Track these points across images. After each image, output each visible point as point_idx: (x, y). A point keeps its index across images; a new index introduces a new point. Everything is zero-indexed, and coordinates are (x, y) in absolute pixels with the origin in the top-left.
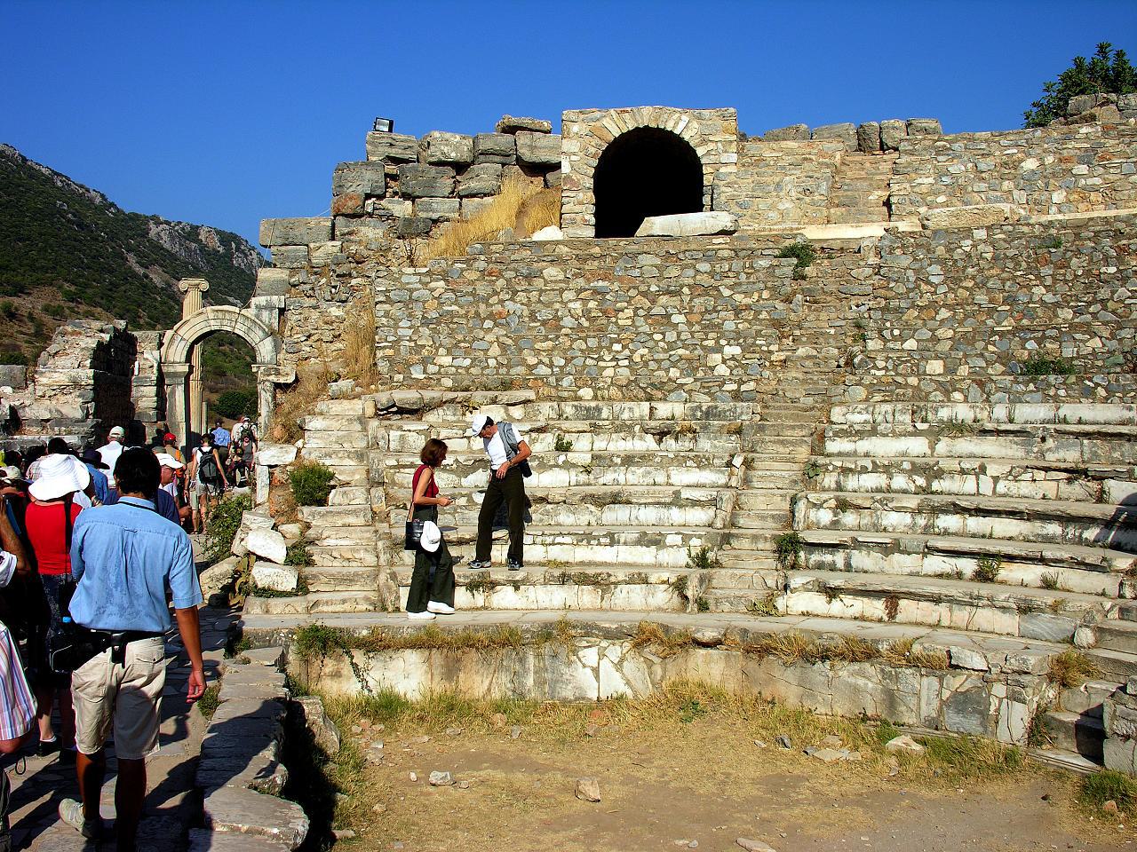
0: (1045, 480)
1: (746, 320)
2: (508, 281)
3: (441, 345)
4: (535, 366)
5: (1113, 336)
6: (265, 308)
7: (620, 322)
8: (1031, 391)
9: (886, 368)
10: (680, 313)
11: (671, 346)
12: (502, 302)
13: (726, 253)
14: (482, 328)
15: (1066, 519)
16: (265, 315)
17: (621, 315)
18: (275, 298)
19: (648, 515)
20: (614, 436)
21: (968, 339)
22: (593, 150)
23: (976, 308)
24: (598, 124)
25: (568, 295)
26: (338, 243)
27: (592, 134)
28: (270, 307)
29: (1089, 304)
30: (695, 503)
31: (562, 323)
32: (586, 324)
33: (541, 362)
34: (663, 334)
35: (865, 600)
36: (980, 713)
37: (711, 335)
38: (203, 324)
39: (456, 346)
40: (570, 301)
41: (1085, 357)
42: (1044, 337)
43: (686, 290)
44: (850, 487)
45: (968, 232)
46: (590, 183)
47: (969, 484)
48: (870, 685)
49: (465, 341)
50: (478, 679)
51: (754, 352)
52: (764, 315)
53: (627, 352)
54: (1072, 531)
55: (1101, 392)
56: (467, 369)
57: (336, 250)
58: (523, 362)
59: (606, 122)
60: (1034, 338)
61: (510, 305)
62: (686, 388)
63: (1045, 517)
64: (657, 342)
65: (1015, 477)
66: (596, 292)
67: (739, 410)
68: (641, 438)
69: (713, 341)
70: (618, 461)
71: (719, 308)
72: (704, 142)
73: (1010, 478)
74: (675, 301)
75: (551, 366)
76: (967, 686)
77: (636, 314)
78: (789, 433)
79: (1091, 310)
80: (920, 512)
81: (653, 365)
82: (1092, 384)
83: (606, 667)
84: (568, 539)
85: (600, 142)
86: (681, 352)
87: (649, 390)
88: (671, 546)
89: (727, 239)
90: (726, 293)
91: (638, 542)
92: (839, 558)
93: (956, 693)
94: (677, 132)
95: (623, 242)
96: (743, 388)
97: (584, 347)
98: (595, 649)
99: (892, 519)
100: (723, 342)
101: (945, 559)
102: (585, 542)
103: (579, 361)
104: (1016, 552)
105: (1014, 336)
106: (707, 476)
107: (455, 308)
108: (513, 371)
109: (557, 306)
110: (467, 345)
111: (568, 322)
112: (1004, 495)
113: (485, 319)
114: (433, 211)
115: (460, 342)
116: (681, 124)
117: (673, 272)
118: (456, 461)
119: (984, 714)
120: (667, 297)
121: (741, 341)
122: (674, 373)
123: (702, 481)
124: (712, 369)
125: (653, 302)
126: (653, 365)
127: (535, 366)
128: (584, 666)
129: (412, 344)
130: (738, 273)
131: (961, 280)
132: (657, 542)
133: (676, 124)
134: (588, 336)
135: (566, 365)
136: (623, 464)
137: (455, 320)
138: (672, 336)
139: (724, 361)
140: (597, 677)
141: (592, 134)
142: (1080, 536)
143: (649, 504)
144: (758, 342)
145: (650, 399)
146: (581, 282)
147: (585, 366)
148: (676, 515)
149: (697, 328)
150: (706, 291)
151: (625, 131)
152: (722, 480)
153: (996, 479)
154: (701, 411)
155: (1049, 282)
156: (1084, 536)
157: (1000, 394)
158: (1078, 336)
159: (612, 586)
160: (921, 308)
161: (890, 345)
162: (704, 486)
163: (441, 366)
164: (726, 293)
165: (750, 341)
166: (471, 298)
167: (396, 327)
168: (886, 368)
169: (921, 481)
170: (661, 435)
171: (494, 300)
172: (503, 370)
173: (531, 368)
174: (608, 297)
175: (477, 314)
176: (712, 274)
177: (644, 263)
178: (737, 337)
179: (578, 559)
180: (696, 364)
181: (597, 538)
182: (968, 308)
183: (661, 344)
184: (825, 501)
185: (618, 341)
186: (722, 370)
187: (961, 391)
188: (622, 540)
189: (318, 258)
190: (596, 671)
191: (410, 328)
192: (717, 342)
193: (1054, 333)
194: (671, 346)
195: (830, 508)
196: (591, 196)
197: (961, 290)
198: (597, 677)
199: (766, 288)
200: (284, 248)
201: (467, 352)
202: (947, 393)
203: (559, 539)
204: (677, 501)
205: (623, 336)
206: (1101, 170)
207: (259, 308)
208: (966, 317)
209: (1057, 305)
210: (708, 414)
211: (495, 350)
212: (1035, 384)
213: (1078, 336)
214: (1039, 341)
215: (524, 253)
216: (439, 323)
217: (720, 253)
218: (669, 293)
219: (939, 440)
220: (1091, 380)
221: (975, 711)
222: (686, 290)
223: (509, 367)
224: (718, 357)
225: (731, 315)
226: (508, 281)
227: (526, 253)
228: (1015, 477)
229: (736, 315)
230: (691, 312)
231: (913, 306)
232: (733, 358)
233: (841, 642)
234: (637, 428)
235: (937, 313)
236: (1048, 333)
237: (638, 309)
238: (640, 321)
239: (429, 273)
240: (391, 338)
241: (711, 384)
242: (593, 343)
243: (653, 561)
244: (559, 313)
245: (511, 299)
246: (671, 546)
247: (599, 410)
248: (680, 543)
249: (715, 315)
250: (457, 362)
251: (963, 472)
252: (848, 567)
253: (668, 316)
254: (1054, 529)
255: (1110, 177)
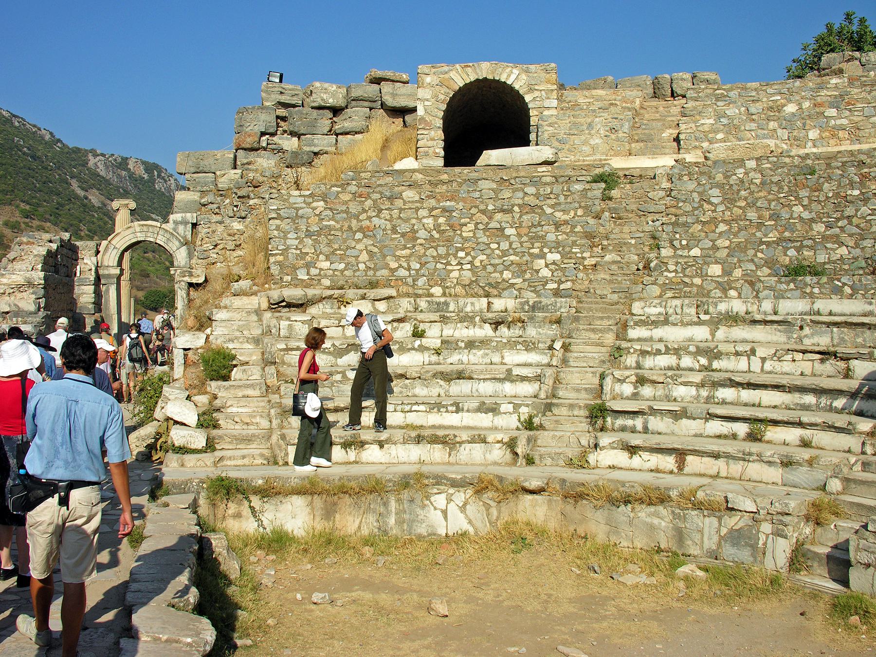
0: (803, 360)
1: (564, 233)
2: (375, 201)
3: (321, 253)
4: (396, 269)
5: (857, 245)
6: (181, 223)
7: (464, 234)
8: (792, 290)
9: (676, 271)
10: (512, 227)
11: (505, 253)
12: (369, 218)
13: (548, 179)
14: (354, 239)
15: (819, 392)
16: (181, 228)
17: (464, 228)
18: (189, 215)
19: (486, 388)
20: (459, 325)
21: (741, 248)
22: (442, 97)
23: (748, 223)
24: (446, 76)
25: (423, 213)
26: (239, 171)
27: (441, 84)
28: (184, 222)
29: (838, 220)
30: (524, 379)
31: (417, 235)
32: (437, 236)
33: (400, 266)
34: (498, 244)
35: (660, 456)
36: (751, 546)
37: (536, 245)
38: (131, 236)
39: (333, 253)
40: (424, 217)
41: (834, 262)
42: (802, 247)
43: (516, 209)
44: (647, 366)
45: (741, 162)
46: (439, 123)
47: (742, 364)
48: (663, 524)
49: (340, 249)
50: (350, 519)
51: (570, 258)
52: (578, 229)
53: (469, 258)
54: (824, 401)
55: (847, 290)
56: (342, 271)
57: (237, 176)
58: (386, 267)
59: (453, 74)
60: (794, 247)
61: (376, 221)
62: (517, 287)
63: (802, 390)
64: (493, 250)
65: (779, 358)
66: (444, 210)
67: (558, 305)
68: (481, 327)
69: (538, 250)
70: (462, 345)
71: (543, 223)
72: (531, 90)
73: (775, 358)
74: (508, 217)
75: (409, 269)
76: (741, 524)
77: (476, 228)
78: (598, 322)
79: (840, 224)
80: (703, 386)
81: (490, 269)
82: (840, 284)
83: (453, 509)
84: (422, 408)
85: (448, 91)
86: (512, 258)
87: (487, 288)
88: (505, 413)
89: (549, 168)
90: (549, 211)
91: (479, 410)
92: (639, 423)
93: (731, 531)
94: (509, 82)
95: (466, 170)
96: (562, 287)
97: (435, 254)
98: (444, 496)
99: (680, 391)
100: (546, 250)
101: (723, 423)
102: (436, 410)
103: (431, 266)
104: (780, 418)
105: (778, 245)
106: (533, 357)
107: (332, 223)
108: (378, 273)
109: (414, 221)
110: (342, 252)
111: (422, 234)
112: (770, 372)
113: (356, 232)
114: (315, 146)
115: (336, 250)
116: (513, 76)
117: (506, 194)
118: (333, 345)
119: (754, 547)
120: (501, 214)
121: (560, 249)
122: (507, 275)
123: (530, 361)
124: (537, 271)
125: (490, 218)
126: (490, 269)
127: (396, 269)
128: (435, 509)
129: (298, 252)
130: (558, 195)
131: (736, 201)
132: (494, 410)
133: (509, 76)
134: (438, 246)
135: (421, 268)
136: (466, 348)
137: (332, 232)
138: (505, 245)
139: (547, 266)
140: (446, 518)
141: (441, 84)
142: (831, 405)
143: (487, 379)
144: (574, 250)
145: (487, 295)
146: (433, 202)
147: (436, 269)
148: (508, 388)
149: (525, 239)
150: (533, 209)
151: (468, 81)
152: (545, 360)
153: (764, 360)
154: (529, 305)
155: (806, 202)
156: (834, 405)
157: (767, 292)
158: (829, 245)
159: (458, 445)
160: (704, 223)
161: (679, 252)
162: (530, 365)
163: (321, 269)
164: (549, 211)
165: (568, 249)
166: (345, 215)
167: (285, 238)
168: (676, 271)
169: (703, 361)
170: (497, 324)
171: (363, 216)
172: (371, 273)
173: (393, 271)
174: (454, 214)
175: (350, 228)
176: (537, 196)
177: (483, 187)
178: (557, 246)
179: (430, 423)
180: (524, 268)
181: (445, 406)
182: (741, 223)
183: (497, 252)
184: (627, 377)
185: (462, 250)
186: (545, 273)
187: (736, 289)
188: (465, 408)
189: (223, 183)
190: (445, 513)
191: (296, 239)
192: (541, 250)
193: (810, 243)
194: (505, 253)
195: (631, 383)
196: (440, 134)
197: (735, 209)
198: (446, 518)
199: (580, 207)
200: (196, 175)
201: (342, 258)
202: (725, 291)
203: (415, 408)
204: (509, 377)
205: (466, 245)
206: (847, 113)
207: (176, 223)
208: (740, 230)
209: (812, 220)
210: (534, 308)
211: (364, 257)
212: (795, 284)
213: (829, 245)
214: (798, 250)
215: (387, 179)
216: (319, 235)
217: (544, 179)
218: (502, 211)
219: (718, 328)
220: (839, 280)
221: (747, 544)
222: (516, 209)
223: (375, 270)
224: (542, 262)
225: (552, 228)
226: (375, 201)
227: (389, 179)
228: (779, 358)
229: (557, 229)
230: (520, 226)
231: (698, 221)
232: (554, 263)
233: (640, 490)
234: (477, 319)
235: (716, 227)
236: (805, 243)
237: (478, 223)
238: (480, 234)
239: (311, 195)
240: (281, 247)
241: (536, 284)
242: (442, 251)
243: (490, 425)
244: (415, 227)
245: (377, 216)
246: (505, 413)
247: (447, 304)
248: (511, 410)
249: (539, 228)
250: (334, 266)
251: (737, 354)
252: (646, 430)
253: (502, 229)
254: (810, 399)
255: (855, 118)
